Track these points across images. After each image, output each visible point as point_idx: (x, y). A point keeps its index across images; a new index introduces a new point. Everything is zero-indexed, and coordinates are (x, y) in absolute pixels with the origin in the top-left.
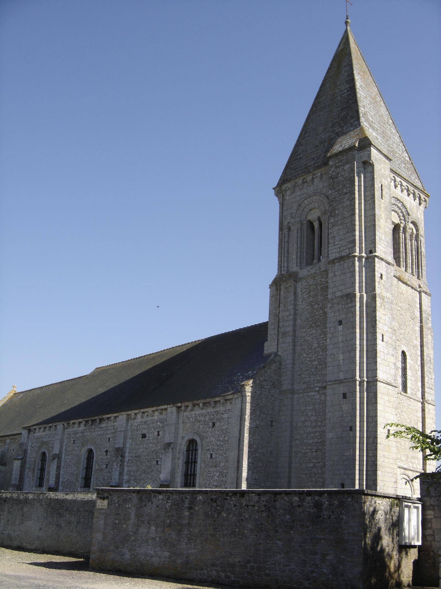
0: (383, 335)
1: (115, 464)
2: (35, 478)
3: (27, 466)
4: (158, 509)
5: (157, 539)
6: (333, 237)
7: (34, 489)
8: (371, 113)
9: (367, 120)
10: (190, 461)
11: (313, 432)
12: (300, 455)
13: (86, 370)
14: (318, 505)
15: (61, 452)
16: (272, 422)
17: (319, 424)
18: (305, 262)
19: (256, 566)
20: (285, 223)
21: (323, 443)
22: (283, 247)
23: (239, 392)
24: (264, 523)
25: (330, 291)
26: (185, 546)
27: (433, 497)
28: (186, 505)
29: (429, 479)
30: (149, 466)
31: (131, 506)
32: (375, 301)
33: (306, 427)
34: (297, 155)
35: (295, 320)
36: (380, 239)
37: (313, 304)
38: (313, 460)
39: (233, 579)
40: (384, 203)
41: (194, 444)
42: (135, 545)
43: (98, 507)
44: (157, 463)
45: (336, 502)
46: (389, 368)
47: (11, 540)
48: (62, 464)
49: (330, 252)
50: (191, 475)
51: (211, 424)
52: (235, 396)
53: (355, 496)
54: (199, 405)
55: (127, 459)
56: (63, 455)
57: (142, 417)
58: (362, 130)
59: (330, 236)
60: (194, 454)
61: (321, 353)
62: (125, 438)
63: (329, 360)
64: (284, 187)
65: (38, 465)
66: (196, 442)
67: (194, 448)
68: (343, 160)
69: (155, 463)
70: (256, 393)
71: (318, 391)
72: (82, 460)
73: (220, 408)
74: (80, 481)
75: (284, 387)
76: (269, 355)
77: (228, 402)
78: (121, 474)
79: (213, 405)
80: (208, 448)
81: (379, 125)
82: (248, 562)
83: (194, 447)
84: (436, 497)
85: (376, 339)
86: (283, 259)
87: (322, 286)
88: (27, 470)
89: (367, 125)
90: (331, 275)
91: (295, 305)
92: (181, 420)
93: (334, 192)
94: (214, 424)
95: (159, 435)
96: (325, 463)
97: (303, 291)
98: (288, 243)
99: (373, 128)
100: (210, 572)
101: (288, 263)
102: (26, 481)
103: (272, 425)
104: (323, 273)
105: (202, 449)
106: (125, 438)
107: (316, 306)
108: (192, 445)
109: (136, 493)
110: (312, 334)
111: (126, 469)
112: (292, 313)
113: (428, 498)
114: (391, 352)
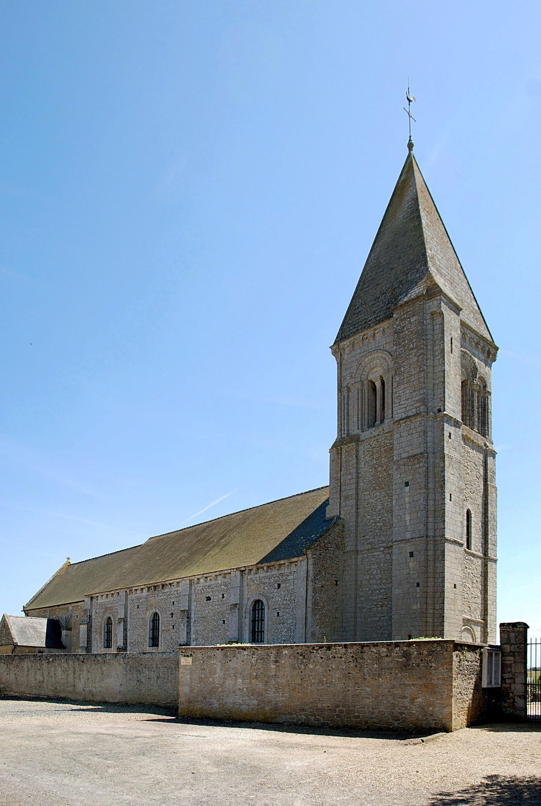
0: (451, 495)
1: (182, 625)
2: (103, 640)
3: (93, 630)
4: (243, 663)
5: (244, 689)
6: (399, 396)
7: (103, 649)
8: (438, 256)
9: (434, 265)
10: (257, 619)
11: (378, 589)
12: (365, 610)
13: (142, 540)
14: (407, 655)
15: (126, 616)
16: (337, 581)
17: (384, 581)
18: (366, 424)
19: (344, 709)
20: (344, 384)
21: (389, 599)
22: (343, 409)
23: (304, 555)
24: (352, 672)
25: (395, 452)
26: (273, 695)
27: (513, 644)
28: (272, 658)
29: (509, 628)
30: (215, 625)
31: (216, 662)
32: (444, 461)
33: (370, 584)
34: (356, 309)
35: (357, 483)
36: (450, 397)
37: (377, 466)
38: (378, 615)
39: (322, 721)
40: (453, 358)
41: (260, 604)
42: (223, 696)
43: (182, 664)
44: (224, 623)
45: (425, 652)
46: (456, 527)
47: (93, 696)
48: (129, 627)
49: (395, 413)
50: (258, 632)
51: (276, 585)
52: (301, 558)
53: (445, 645)
54: (263, 568)
55: (192, 620)
56: (129, 619)
57: (206, 581)
58: (431, 277)
59: (395, 396)
60: (260, 613)
61: (386, 515)
62: (190, 601)
63: (395, 520)
64: (342, 344)
65: (104, 628)
66: (262, 602)
67: (260, 608)
68: (410, 311)
69: (222, 622)
70: (321, 555)
71: (383, 551)
72: (148, 622)
73: (285, 570)
74: (148, 642)
75: (348, 549)
76: (331, 519)
77: (293, 565)
78: (188, 633)
79: (277, 568)
80: (274, 607)
81: (447, 270)
82: (338, 706)
83: (260, 607)
84: (516, 644)
85: (444, 499)
86: (342, 421)
87: (386, 448)
88: (93, 634)
89: (434, 270)
90: (396, 436)
91: (357, 468)
92: (245, 583)
93: (399, 348)
94: (279, 586)
95: (223, 597)
96: (391, 616)
97: (365, 455)
98: (348, 405)
99: (441, 274)
100: (299, 716)
101: (348, 426)
102: (94, 643)
103: (337, 585)
104: (387, 435)
105: (268, 608)
106: (190, 601)
107: (379, 469)
108: (258, 606)
109: (220, 650)
110: (376, 496)
111: (192, 628)
112: (354, 477)
113: (508, 646)
114: (458, 510)
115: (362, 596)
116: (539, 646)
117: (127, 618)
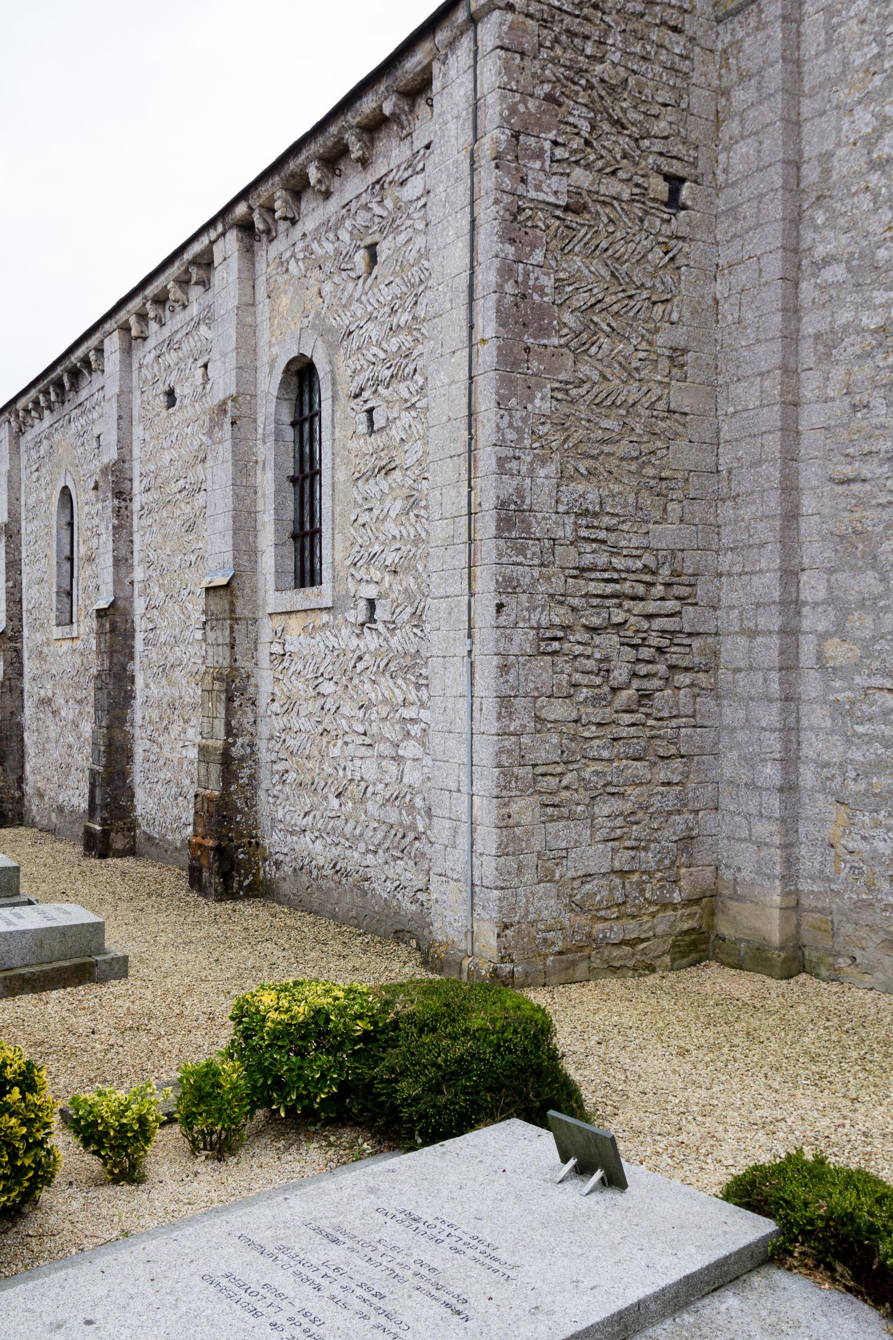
16: (675, 182)
115: (827, 261)
116: (57, 761)
117: (18, 521)
